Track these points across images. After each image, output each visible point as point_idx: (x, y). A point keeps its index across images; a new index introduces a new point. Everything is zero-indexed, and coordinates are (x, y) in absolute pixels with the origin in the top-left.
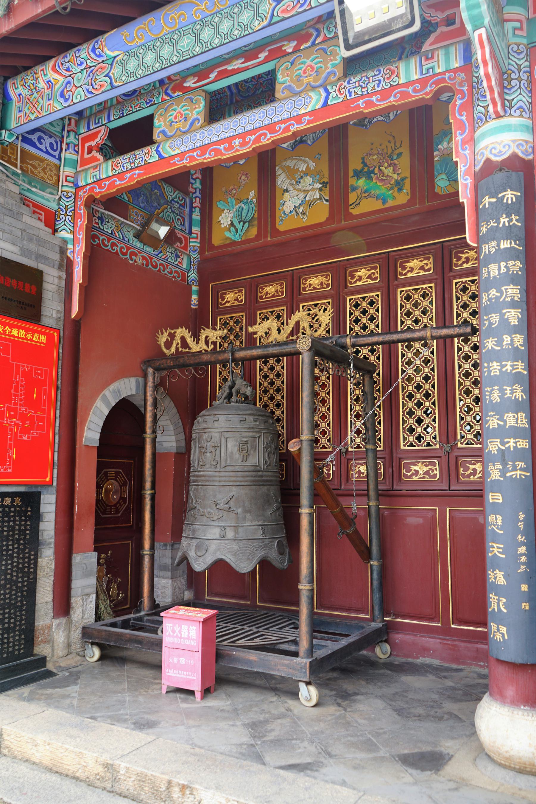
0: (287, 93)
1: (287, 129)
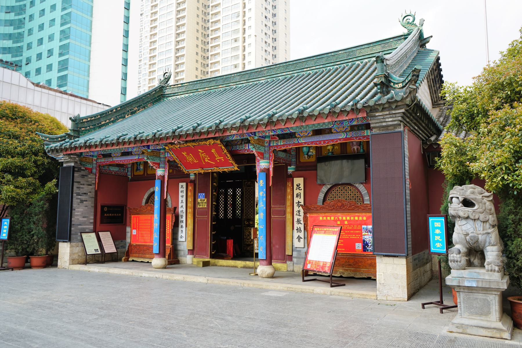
0: (335, 132)
1: (336, 142)
